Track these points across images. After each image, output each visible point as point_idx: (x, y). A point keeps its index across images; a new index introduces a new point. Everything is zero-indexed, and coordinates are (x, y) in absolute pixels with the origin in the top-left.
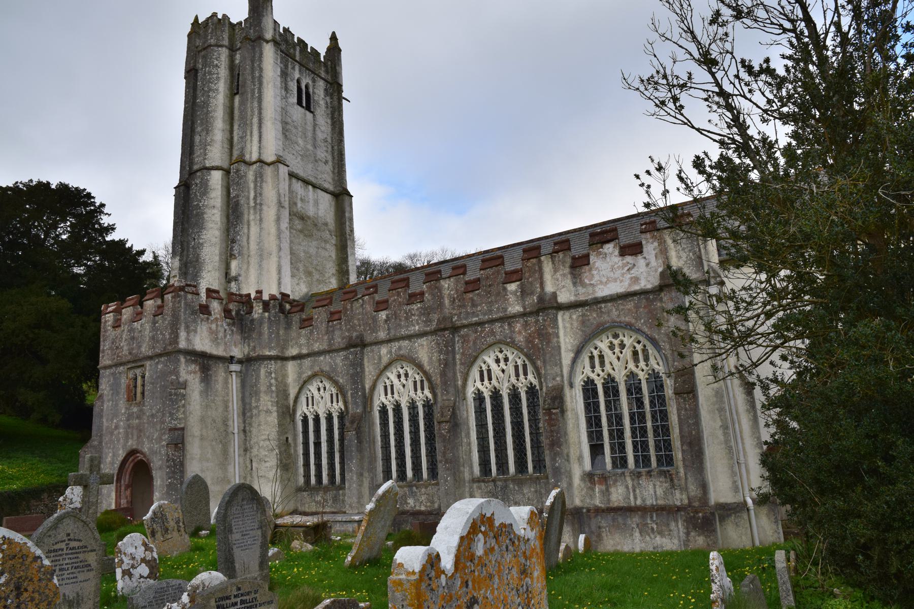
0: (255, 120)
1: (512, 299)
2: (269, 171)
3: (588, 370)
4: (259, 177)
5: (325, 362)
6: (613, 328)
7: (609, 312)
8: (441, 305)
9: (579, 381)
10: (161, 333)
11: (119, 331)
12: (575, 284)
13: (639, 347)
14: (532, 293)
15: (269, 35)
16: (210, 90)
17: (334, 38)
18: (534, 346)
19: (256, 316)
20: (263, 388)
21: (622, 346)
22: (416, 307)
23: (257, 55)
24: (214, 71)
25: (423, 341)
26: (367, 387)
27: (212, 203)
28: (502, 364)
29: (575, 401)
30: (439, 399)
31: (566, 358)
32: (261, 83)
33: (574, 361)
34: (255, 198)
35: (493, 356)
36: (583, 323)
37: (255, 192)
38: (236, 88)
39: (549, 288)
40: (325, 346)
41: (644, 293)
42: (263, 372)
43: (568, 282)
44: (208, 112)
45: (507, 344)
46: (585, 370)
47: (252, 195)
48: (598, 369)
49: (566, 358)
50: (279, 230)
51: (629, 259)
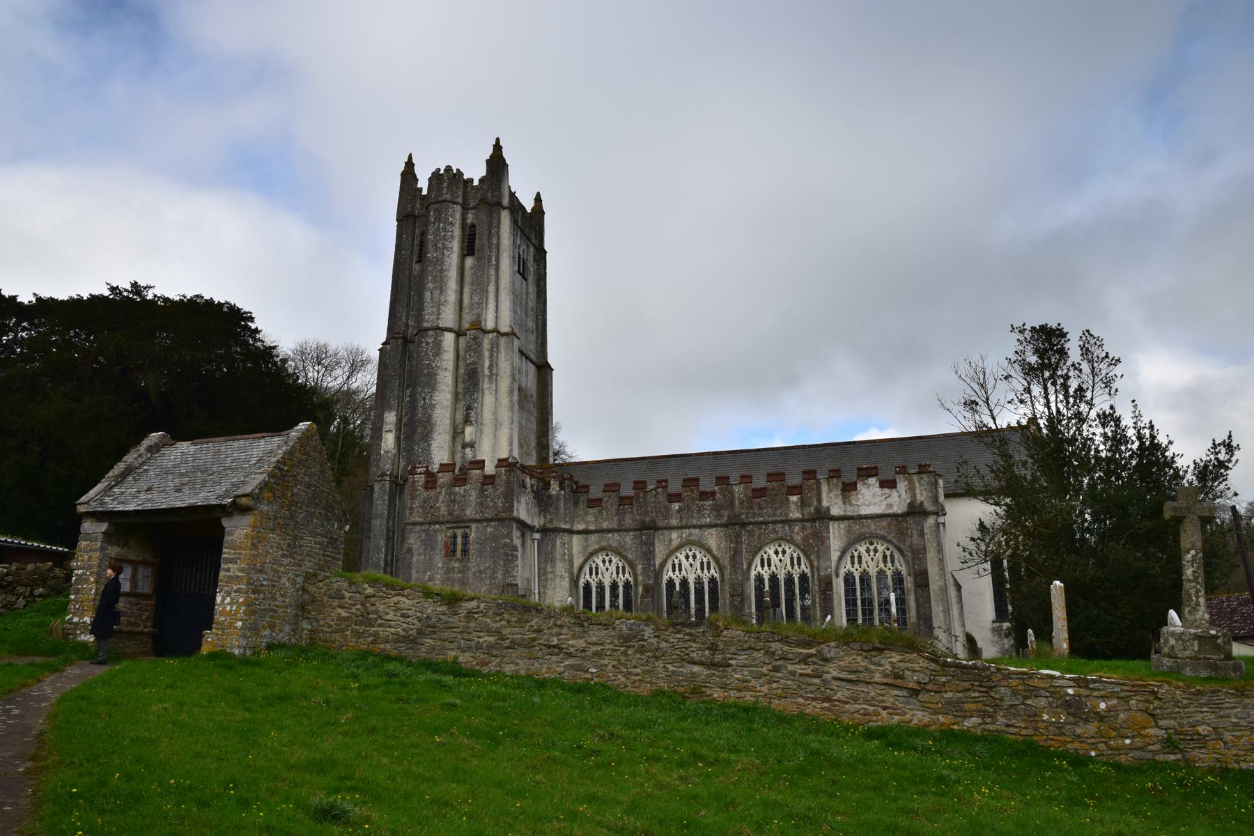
0: (492, 288)
1: (793, 507)
2: (503, 340)
3: (849, 565)
4: (494, 347)
5: (613, 539)
6: (870, 538)
7: (868, 527)
8: (732, 504)
9: (842, 572)
10: (492, 501)
11: (432, 493)
12: (844, 503)
13: (888, 553)
14: (810, 505)
15: (506, 202)
16: (445, 248)
17: (538, 199)
18: (809, 544)
19: (554, 493)
20: (558, 557)
21: (876, 551)
22: (708, 503)
23: (495, 222)
24: (449, 228)
25: (713, 531)
26: (657, 563)
27: (444, 364)
28: (780, 555)
29: (839, 587)
30: (727, 576)
31: (835, 555)
32: (498, 251)
33: (840, 558)
34: (491, 367)
35: (773, 549)
36: (848, 531)
37: (491, 361)
38: (469, 248)
39: (825, 503)
40: (614, 525)
41: (895, 515)
42: (558, 542)
43: (839, 501)
44: (442, 271)
45: (788, 541)
46: (846, 566)
47: (487, 363)
48: (856, 565)
49: (835, 555)
50: (511, 401)
51: (886, 490)
